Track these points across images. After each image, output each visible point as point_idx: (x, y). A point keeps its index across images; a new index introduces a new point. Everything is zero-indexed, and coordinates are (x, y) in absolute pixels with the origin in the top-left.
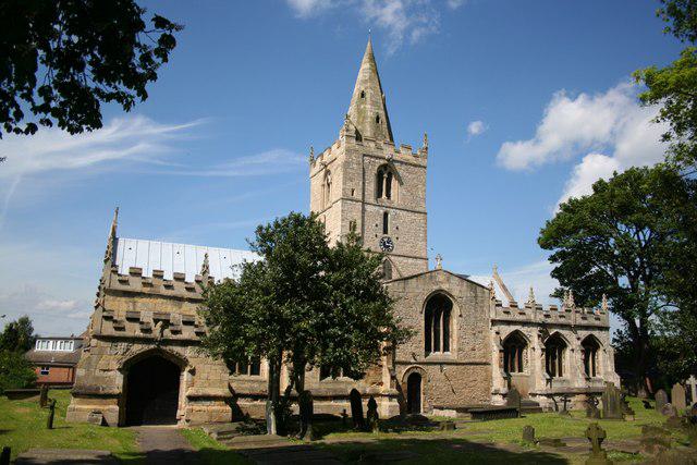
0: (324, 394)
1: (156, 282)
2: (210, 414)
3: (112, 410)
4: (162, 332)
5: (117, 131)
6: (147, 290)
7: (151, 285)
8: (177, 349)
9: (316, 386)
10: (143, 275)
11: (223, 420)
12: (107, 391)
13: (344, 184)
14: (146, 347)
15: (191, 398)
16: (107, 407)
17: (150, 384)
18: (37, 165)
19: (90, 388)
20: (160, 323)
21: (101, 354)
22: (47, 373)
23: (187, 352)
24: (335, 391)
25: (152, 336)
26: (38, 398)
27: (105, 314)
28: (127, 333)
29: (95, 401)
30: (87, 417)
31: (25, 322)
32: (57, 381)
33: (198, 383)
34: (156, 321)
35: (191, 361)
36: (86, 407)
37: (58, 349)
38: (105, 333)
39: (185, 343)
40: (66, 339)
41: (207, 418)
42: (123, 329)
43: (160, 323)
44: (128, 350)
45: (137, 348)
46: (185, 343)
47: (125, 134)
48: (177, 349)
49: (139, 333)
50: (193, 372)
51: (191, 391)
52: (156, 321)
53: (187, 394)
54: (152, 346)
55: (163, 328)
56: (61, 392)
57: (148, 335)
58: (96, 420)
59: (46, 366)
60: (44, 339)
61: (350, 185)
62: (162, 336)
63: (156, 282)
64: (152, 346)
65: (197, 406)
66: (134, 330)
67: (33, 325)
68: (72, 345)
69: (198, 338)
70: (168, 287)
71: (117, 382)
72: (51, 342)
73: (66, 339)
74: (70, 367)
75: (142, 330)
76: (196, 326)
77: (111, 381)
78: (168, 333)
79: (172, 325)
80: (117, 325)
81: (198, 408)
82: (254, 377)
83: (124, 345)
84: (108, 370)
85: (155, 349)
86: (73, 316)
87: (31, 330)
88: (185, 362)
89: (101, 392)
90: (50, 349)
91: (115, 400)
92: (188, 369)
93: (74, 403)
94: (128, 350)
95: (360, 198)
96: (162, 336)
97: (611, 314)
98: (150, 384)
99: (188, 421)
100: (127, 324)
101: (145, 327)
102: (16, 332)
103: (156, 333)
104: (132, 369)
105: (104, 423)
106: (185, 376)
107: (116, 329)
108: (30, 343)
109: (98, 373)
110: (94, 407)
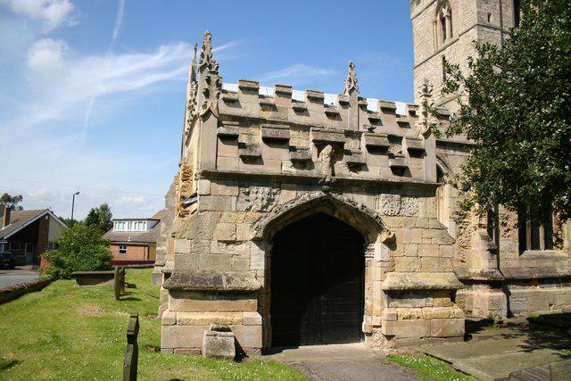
0: (527, 275)
1: (281, 103)
2: (428, 320)
3: (248, 322)
4: (332, 165)
5: (165, 56)
6: (268, 115)
7: (273, 107)
8: (361, 200)
9: (514, 264)
10: (261, 92)
11: (451, 332)
12: (237, 284)
13: (479, 6)
14: (306, 196)
15: (394, 294)
16: (237, 317)
17: (314, 270)
18: (104, 89)
19: (201, 279)
20: (328, 149)
21: (218, 211)
22: (124, 252)
23: (378, 205)
24: (540, 271)
25: (313, 173)
26: (112, 282)
27: (222, 130)
28: (268, 168)
29: (217, 303)
30: (203, 339)
31: (105, 208)
32: (135, 259)
33: (402, 264)
34: (320, 145)
35: (387, 222)
36: (197, 316)
37: (133, 230)
38: (223, 168)
39: (375, 188)
40: (140, 220)
41: (422, 331)
42: (257, 160)
43: (328, 149)
44: (270, 201)
45: (288, 198)
46: (375, 188)
47: (169, 59)
48: (361, 200)
49: (288, 169)
50: (391, 243)
51: (391, 281)
52: (320, 145)
53: (386, 285)
54: (317, 194)
55: (334, 157)
56: (140, 271)
57: (305, 172)
58: (224, 346)
59: (123, 246)
60: (120, 221)
61: (486, 8)
62: (333, 174)
63: (281, 103)
64: (317, 194)
65: (404, 308)
66: (278, 162)
67: (112, 211)
68: (146, 225)
69: (396, 179)
70: (300, 111)
71: (253, 266)
72: (127, 223)
73: (140, 220)
74: (145, 246)
75: (295, 162)
76: (392, 156)
77: (243, 263)
78: (342, 169)
79: (349, 153)
80: (247, 153)
81: (407, 313)
82: (535, 252)
83: (263, 192)
84: (234, 242)
85: (321, 200)
86: (144, 208)
87: (110, 215)
88: (376, 225)
89: (225, 286)
90: (126, 229)
91: (254, 302)
92: (383, 236)
93: (172, 309)
94: (270, 201)
95: (498, 25)
96: (333, 174)
97: (255, 247)
98: (314, 270)
99: (389, 337)
100: (266, 152)
101: (299, 156)
102: (97, 216)
103: (321, 167)
104: (281, 239)
105: (240, 355)
106: (377, 252)
107: (246, 159)
108: (108, 226)
109: (215, 248)
110: (221, 316)
